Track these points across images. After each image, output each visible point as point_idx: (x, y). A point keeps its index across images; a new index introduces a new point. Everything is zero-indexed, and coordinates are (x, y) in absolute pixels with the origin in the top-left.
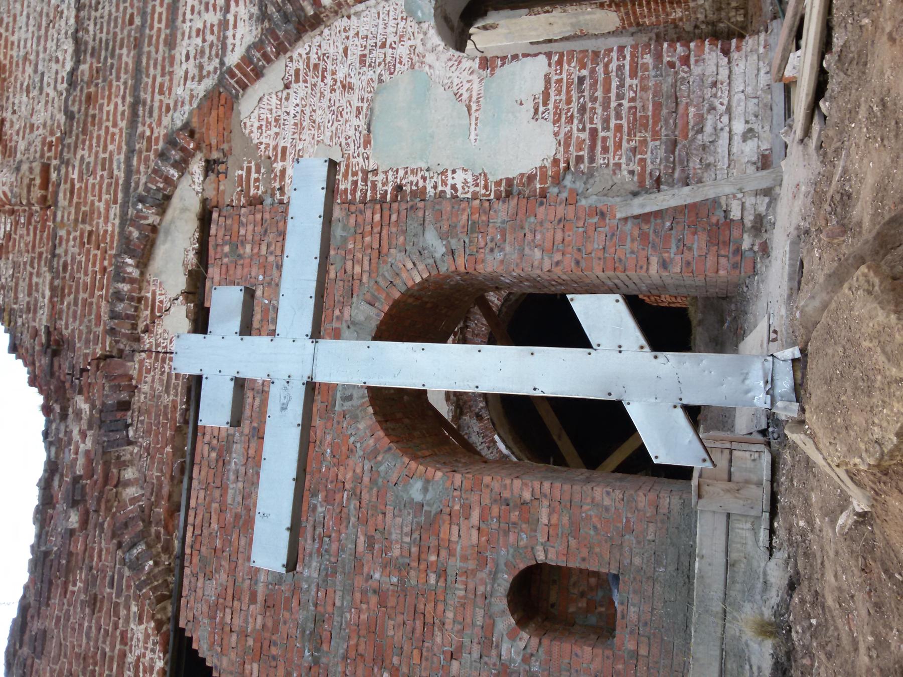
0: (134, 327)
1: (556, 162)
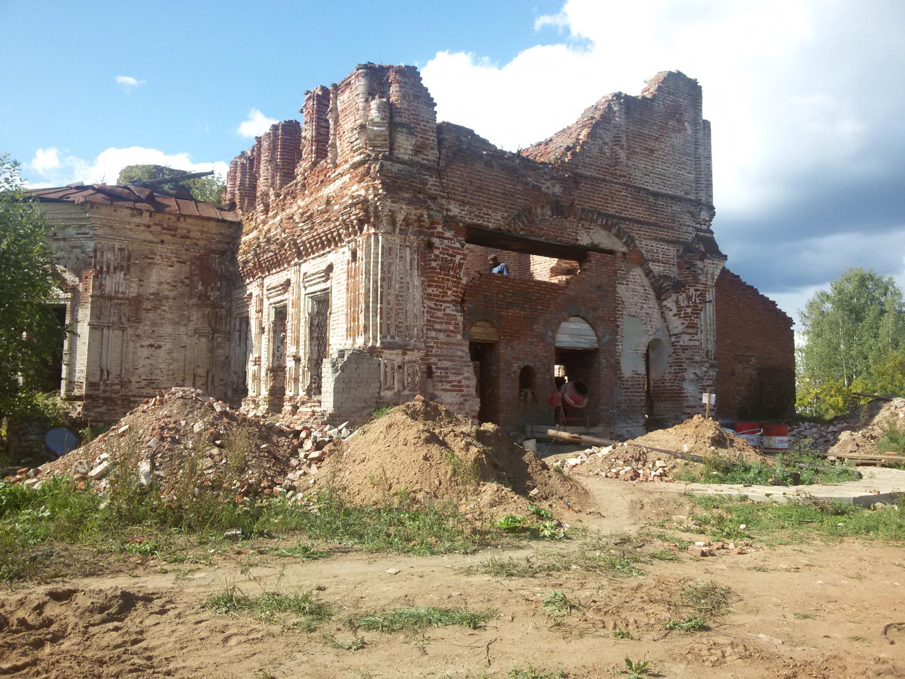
0: (583, 220)
1: (623, 377)
